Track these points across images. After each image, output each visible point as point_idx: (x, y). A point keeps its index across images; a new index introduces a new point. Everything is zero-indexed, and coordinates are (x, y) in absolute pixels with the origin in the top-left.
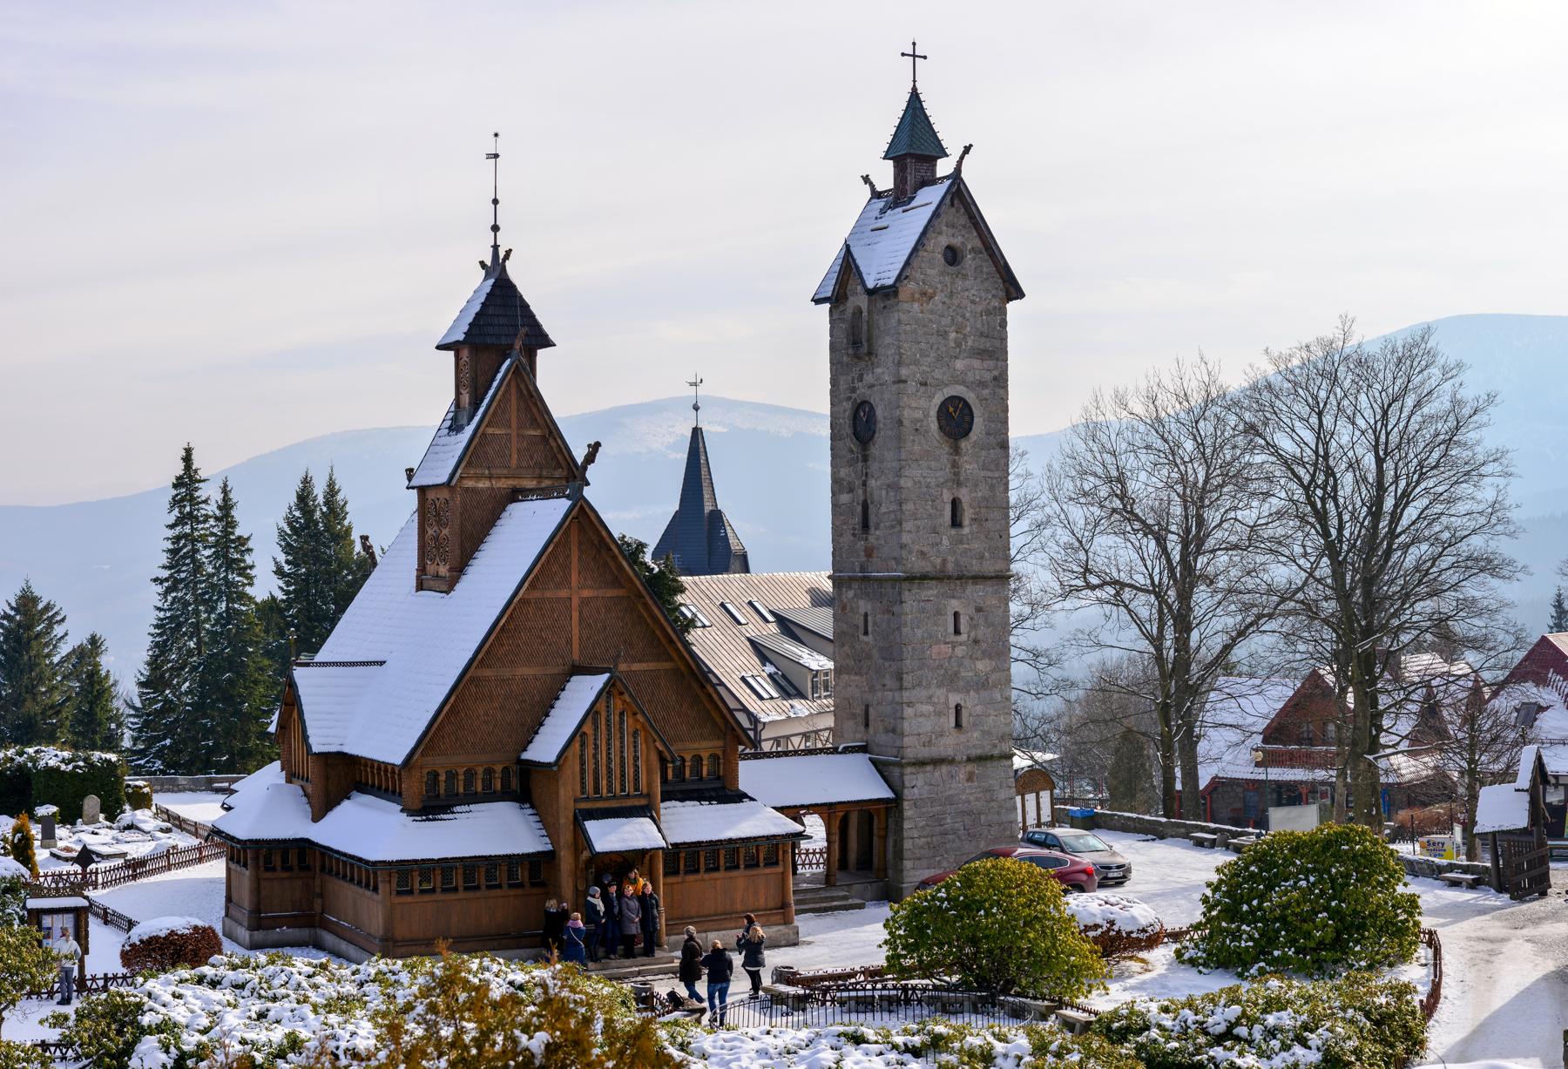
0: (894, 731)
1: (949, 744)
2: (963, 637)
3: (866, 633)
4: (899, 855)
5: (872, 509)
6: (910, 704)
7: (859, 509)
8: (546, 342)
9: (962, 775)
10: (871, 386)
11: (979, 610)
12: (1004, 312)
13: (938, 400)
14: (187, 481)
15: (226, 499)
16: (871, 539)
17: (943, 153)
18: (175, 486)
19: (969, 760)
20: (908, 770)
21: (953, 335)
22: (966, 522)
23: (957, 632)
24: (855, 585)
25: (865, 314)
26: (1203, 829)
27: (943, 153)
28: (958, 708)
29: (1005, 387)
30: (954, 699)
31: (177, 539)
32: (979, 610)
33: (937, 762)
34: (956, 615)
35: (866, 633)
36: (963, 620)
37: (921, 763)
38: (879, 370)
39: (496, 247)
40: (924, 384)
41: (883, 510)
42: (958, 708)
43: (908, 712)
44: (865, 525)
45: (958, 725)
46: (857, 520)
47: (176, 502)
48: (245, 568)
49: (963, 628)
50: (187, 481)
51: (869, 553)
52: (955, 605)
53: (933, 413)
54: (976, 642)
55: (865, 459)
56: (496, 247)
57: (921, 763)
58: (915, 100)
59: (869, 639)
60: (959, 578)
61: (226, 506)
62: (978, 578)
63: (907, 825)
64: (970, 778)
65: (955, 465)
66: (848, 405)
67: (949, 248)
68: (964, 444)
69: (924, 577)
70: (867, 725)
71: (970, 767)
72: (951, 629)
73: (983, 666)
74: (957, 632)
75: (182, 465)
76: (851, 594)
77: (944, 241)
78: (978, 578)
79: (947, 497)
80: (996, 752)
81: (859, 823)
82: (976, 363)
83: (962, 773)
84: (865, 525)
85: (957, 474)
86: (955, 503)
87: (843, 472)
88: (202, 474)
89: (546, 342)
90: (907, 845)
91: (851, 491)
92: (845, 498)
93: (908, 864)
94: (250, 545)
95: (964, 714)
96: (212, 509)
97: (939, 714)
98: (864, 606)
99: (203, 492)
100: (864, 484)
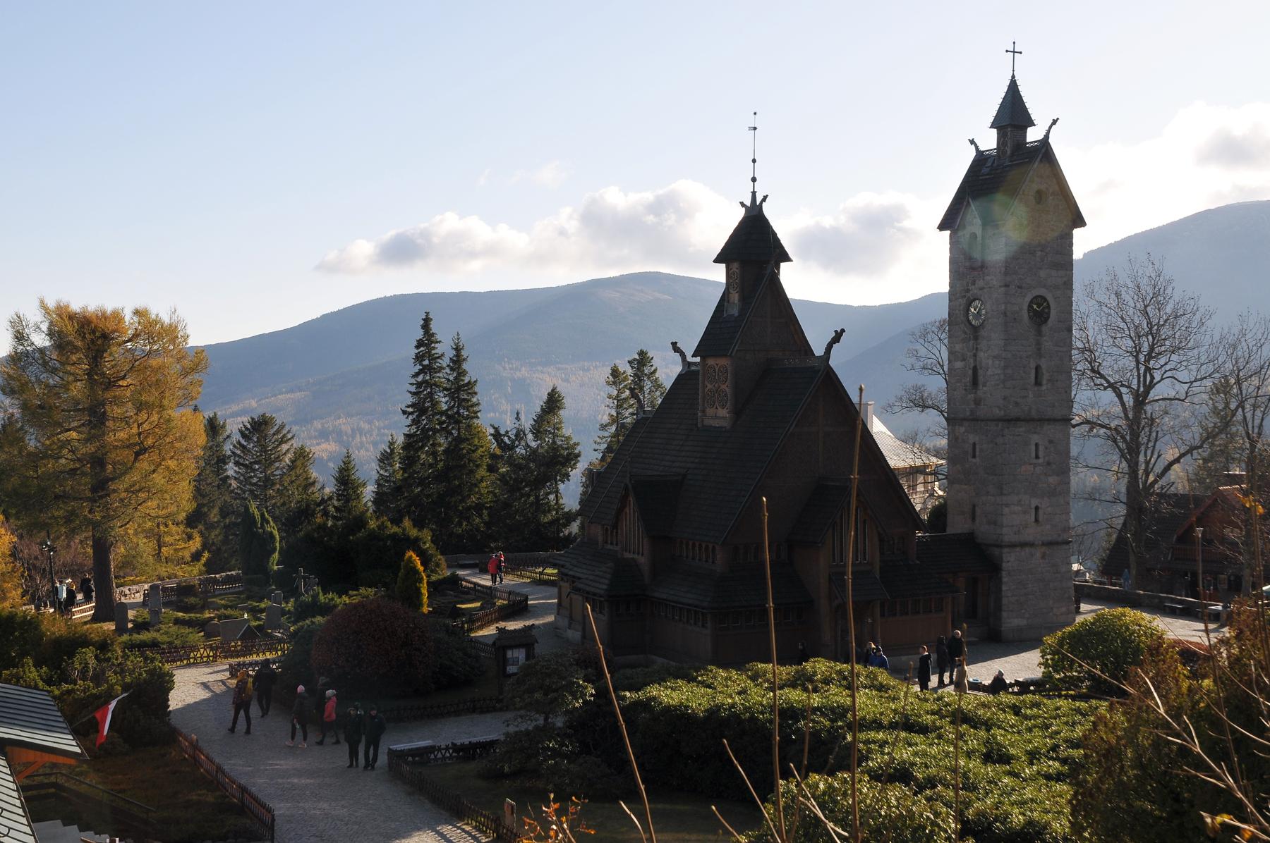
0: (995, 523)
1: (1031, 534)
2: (1041, 461)
3: (974, 456)
4: (999, 608)
5: (980, 372)
6: (1007, 505)
7: (970, 372)
8: (786, 258)
9: (1038, 555)
10: (982, 289)
11: (1051, 442)
12: (1070, 237)
13: (1028, 299)
14: (427, 341)
15: (458, 355)
16: (980, 393)
17: (1031, 123)
18: (417, 347)
19: (1043, 544)
20: (1005, 550)
21: (1039, 253)
22: (1044, 382)
23: (1037, 457)
24: (966, 424)
25: (979, 239)
26: (1173, 601)
27: (1031, 123)
28: (1037, 508)
29: (1071, 289)
30: (1035, 502)
31: (419, 385)
32: (1051, 442)
33: (1024, 545)
34: (1037, 445)
35: (974, 456)
36: (1041, 448)
37: (1013, 546)
38: (988, 278)
39: (754, 193)
40: (1020, 287)
41: (989, 373)
42: (1037, 508)
43: (1006, 510)
44: (975, 382)
45: (1037, 520)
46: (968, 379)
47: (419, 358)
48: (472, 406)
49: (1041, 454)
50: (427, 341)
51: (977, 402)
52: (1035, 438)
53: (1025, 307)
54: (1049, 464)
55: (976, 338)
56: (754, 193)
57: (1013, 546)
58: (1013, 88)
59: (977, 460)
60: (1039, 420)
61: (457, 361)
62: (1055, 420)
63: (1004, 588)
64: (1043, 557)
65: (1038, 344)
66: (963, 301)
67: (1039, 193)
68: (1044, 329)
69: (1018, 419)
70: (974, 519)
71: (1044, 549)
72: (1033, 455)
73: (1052, 480)
74: (1037, 457)
75: (419, 334)
76: (962, 429)
77: (1035, 187)
78: (1055, 420)
79: (1033, 365)
80: (1060, 539)
81: (456, 712)
82: (1054, 273)
83: (1038, 553)
84: (975, 382)
85: (1039, 349)
86: (1038, 368)
87: (958, 347)
88: (438, 337)
89: (786, 258)
90: (1005, 601)
91: (964, 360)
92: (959, 364)
93: (1004, 614)
94: (476, 389)
95: (1041, 512)
96: (445, 362)
97: (1025, 512)
98: (972, 438)
99: (439, 349)
100: (975, 355)
